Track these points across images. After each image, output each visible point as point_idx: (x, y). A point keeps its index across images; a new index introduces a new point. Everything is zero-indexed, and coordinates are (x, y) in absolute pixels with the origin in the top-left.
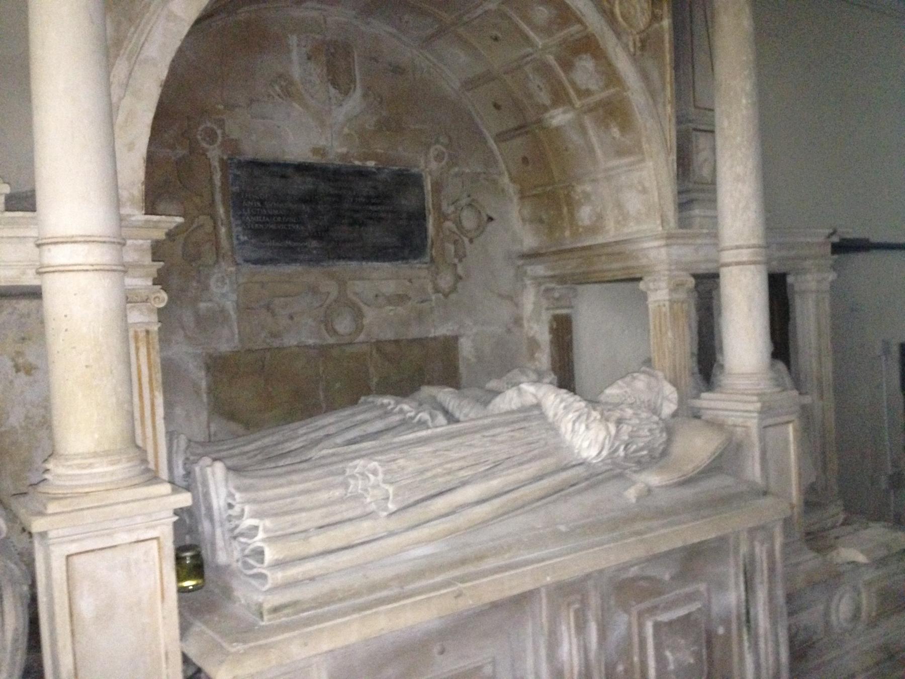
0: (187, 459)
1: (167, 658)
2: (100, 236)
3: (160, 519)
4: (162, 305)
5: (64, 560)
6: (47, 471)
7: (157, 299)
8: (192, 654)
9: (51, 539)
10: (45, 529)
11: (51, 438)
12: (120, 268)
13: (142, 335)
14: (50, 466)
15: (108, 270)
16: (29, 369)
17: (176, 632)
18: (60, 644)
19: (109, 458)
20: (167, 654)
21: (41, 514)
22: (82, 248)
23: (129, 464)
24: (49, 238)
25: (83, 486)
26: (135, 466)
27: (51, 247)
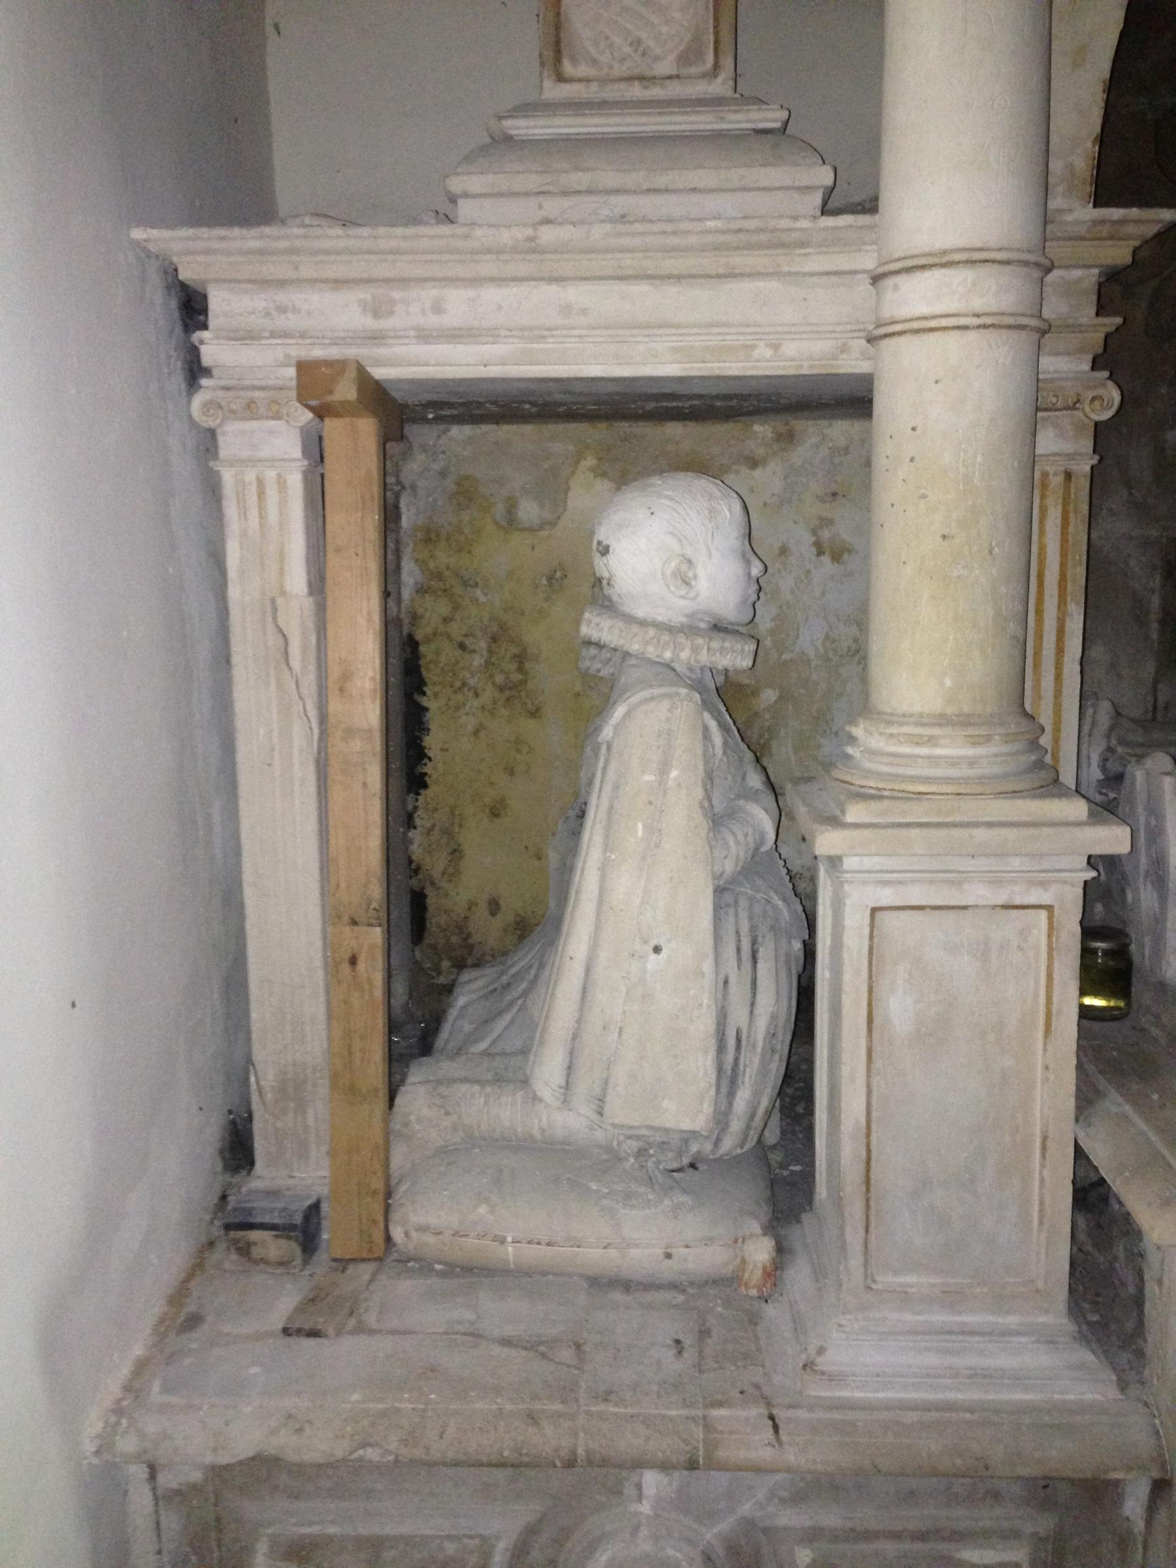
0: (1110, 749)
1: (1044, 1148)
2: (1000, 249)
3: (1060, 871)
4: (1106, 415)
5: (868, 912)
6: (852, 740)
7: (1097, 403)
8: (1101, 1155)
9: (847, 872)
10: (838, 852)
11: (864, 680)
12: (1034, 322)
13: (1056, 481)
14: (858, 731)
15: (1009, 327)
16: (838, 552)
17: (1070, 1104)
18: (845, 1070)
19: (971, 731)
20: (1044, 1139)
21: (835, 821)
22: (961, 277)
23: (1005, 749)
24: (898, 260)
25: (913, 779)
26: (1017, 753)
27: (900, 279)
